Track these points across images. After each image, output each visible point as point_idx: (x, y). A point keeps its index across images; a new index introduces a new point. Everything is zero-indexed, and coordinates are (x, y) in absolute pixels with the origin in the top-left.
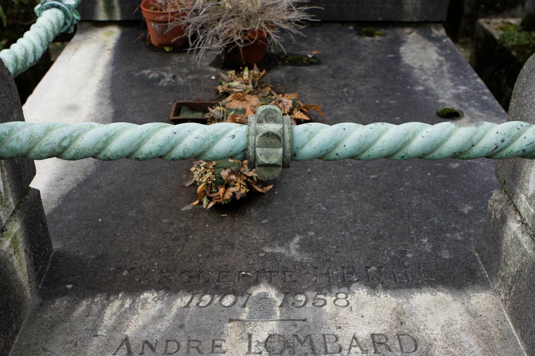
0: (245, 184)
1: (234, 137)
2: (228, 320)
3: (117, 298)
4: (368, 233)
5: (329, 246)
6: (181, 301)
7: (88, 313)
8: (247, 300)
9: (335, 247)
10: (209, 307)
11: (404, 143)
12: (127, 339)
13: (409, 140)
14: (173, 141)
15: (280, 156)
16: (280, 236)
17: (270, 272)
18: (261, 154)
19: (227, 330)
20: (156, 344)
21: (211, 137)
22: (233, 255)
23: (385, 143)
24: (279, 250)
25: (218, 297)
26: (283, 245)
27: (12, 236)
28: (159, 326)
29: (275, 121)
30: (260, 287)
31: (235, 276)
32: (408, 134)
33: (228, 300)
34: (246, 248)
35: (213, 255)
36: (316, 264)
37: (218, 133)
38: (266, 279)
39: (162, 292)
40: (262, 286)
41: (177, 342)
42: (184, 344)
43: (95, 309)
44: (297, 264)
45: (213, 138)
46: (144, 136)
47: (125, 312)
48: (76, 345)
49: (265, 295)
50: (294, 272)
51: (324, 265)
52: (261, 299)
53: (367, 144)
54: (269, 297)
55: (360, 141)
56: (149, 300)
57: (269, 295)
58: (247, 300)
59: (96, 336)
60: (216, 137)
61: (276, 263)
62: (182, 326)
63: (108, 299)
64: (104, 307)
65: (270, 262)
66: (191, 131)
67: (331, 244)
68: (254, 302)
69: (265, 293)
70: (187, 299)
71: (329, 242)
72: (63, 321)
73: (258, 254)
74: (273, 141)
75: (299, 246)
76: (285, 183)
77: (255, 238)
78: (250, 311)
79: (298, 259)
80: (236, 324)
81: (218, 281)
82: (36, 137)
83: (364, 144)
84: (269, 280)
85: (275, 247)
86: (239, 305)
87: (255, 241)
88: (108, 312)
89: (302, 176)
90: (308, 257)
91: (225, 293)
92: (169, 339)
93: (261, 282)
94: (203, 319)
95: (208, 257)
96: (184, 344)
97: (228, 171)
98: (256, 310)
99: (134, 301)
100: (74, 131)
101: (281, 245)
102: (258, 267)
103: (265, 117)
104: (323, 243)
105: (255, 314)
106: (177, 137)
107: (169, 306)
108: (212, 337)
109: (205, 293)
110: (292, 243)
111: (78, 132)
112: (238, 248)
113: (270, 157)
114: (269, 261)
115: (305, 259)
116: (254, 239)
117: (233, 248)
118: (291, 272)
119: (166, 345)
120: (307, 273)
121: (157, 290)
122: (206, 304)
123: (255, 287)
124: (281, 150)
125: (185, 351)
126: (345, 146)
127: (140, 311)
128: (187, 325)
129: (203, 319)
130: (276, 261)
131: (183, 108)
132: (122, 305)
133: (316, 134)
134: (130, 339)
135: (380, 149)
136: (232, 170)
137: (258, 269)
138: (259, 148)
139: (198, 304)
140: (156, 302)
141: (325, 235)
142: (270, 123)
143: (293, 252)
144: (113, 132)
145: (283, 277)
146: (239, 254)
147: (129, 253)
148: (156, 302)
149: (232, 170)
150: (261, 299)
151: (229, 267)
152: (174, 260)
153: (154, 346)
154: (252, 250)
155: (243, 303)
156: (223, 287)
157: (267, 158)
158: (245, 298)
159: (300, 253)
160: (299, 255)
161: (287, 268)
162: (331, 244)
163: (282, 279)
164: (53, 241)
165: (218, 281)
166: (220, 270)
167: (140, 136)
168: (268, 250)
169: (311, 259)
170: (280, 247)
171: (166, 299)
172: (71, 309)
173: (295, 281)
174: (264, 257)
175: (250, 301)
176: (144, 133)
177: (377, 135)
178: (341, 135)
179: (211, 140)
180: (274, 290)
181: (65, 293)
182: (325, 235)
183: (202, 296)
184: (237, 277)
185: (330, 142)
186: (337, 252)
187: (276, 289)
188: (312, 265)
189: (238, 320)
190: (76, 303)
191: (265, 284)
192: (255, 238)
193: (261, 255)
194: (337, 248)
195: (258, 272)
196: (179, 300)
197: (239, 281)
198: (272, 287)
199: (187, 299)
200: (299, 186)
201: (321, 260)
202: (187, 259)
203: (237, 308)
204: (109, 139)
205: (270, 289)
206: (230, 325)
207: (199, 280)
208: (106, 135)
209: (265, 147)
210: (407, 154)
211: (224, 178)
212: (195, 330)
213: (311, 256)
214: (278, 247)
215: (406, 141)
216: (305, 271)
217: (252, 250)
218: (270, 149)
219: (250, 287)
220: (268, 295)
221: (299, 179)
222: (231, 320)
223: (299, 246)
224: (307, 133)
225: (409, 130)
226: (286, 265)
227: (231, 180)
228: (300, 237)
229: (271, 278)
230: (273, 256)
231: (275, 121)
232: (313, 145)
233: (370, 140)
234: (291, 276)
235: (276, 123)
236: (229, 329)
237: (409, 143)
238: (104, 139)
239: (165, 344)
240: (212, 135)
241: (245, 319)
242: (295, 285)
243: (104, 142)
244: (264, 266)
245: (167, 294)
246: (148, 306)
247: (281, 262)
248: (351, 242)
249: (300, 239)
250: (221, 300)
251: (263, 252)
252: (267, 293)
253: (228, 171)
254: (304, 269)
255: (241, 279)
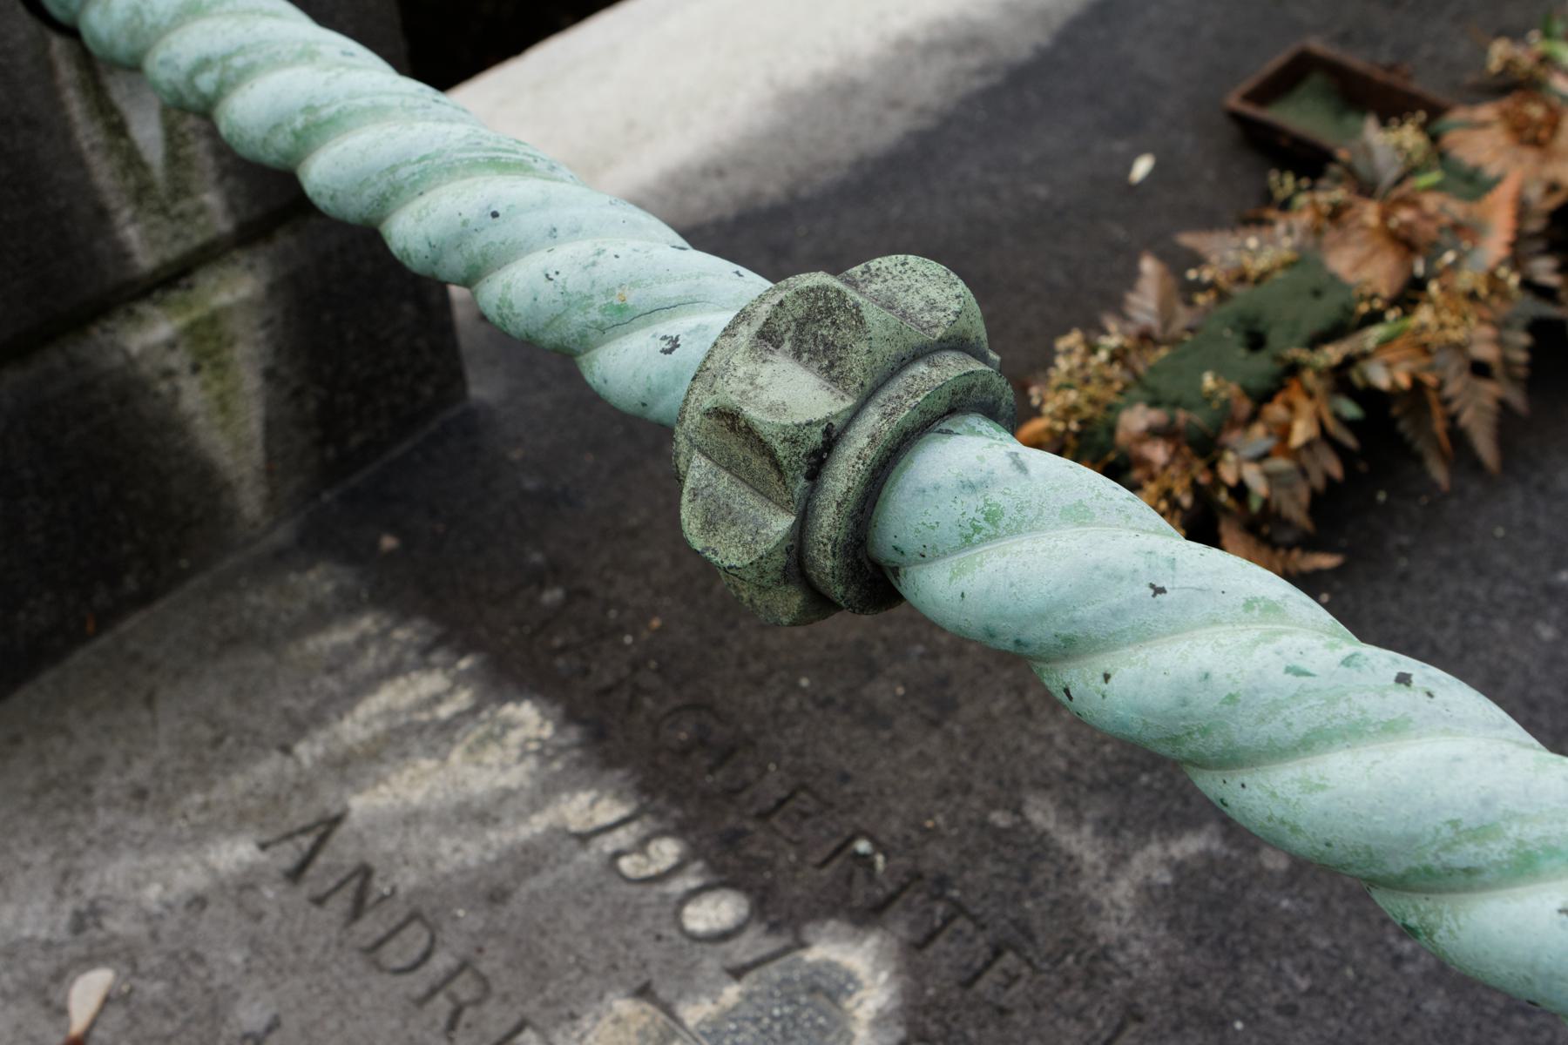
0: (1186, 501)
1: (674, 344)
2: (637, 984)
3: (446, 667)
4: (1519, 1021)
5: (1287, 965)
6: (590, 807)
7: (338, 663)
8: (773, 957)
9: (1303, 984)
10: (635, 890)
11: (1428, 870)
12: (332, 822)
13: (1469, 871)
14: (477, 244)
15: (762, 548)
16: (1148, 788)
17: (959, 909)
18: (695, 493)
19: (598, 1018)
20: (383, 898)
21: (600, 301)
22: (906, 755)
23: (1317, 800)
24: (1083, 845)
25: (700, 873)
26: (1115, 834)
27: (196, 313)
28: (445, 846)
29: (832, 366)
30: (863, 939)
31: (833, 835)
32: (1481, 833)
33: (715, 912)
34: (974, 755)
35: (847, 709)
36: (1151, 1002)
37: (632, 297)
38: (913, 925)
39: (573, 734)
40: (872, 941)
41: (433, 940)
42: (441, 962)
43: (371, 659)
44: (1082, 944)
45: (602, 311)
46: (403, 173)
47: (421, 729)
48: (217, 742)
49: (842, 988)
50: (1036, 970)
51: (1177, 1028)
52: (813, 989)
53: (1217, 742)
54: (849, 1004)
55: (1184, 703)
56: (514, 737)
57: (858, 996)
58: (773, 957)
59: (286, 750)
60: (621, 309)
61: (1016, 886)
62: (497, 896)
63: (426, 651)
64: (395, 670)
65: (1001, 868)
66: (560, 232)
67: (1302, 959)
68: (786, 981)
69: (850, 977)
70: (607, 811)
71: (1306, 946)
72: (268, 643)
73: (992, 805)
74: (757, 463)
75: (1167, 879)
76: (1404, 577)
77: (1049, 738)
78: (735, 1008)
79: (1108, 930)
80: (645, 1019)
81: (763, 816)
82: (149, 19)
83: (1205, 732)
84: (918, 937)
85: (1078, 821)
86: (727, 955)
87: (1035, 749)
88: (387, 697)
89: (1507, 589)
90: (1155, 945)
91: (722, 879)
92: (426, 910)
93: (884, 926)
94: (577, 919)
95: (827, 703)
96: (441, 962)
97: (1156, 416)
98: (756, 1021)
99: (474, 711)
100: (241, 50)
101: (1109, 828)
102: (939, 856)
103: (801, 325)
104: (1275, 934)
105: (737, 1032)
106: (495, 234)
107: (547, 790)
108: (532, 1007)
109: (679, 831)
110: (1155, 850)
111: (252, 57)
112: (949, 737)
113: (722, 527)
114: (1001, 859)
115: (1135, 948)
116: (1037, 737)
117: (935, 724)
118: (1029, 962)
119: (401, 927)
120: (1079, 1015)
121: (571, 716)
122: (643, 873)
123: (846, 928)
124: (781, 524)
125: (420, 989)
126: (1107, 677)
127: (456, 756)
128: (516, 906)
129: (577, 919)
130: (1026, 878)
131: (1317, 79)
132: (437, 699)
133: (1015, 530)
134: (343, 830)
135: (1278, 813)
136: (1172, 421)
137: (927, 865)
138: (703, 461)
139: (618, 854)
140: (521, 759)
141: (1325, 903)
142: (806, 366)
143: (1123, 890)
144: (333, 109)
145: (979, 963)
146: (924, 760)
147: (633, 533)
148: (521, 759)
149: (1172, 421)
150: (813, 989)
151: (848, 789)
152: (719, 643)
153: (371, 899)
154: (987, 777)
155: (748, 959)
156: (753, 850)
157: (709, 525)
158: (770, 945)
159: (1142, 913)
160: (1127, 916)
161: (1031, 938)
162: (1302, 959)
163: (968, 967)
164: (471, 375)
165: (763, 816)
166: (809, 780)
167: (393, 169)
168: (1041, 814)
169: (1157, 966)
170: (1096, 833)
171: (557, 766)
172: (321, 618)
173: (1002, 1011)
174: (998, 834)
175: (774, 971)
176: (409, 162)
177: (1300, 730)
178: (1117, 613)
179: (595, 315)
180: (894, 988)
181: (355, 554)
182: (1325, 903)
183: (662, 834)
184: (835, 843)
185: (1041, 616)
186: (1289, 1010)
187: (904, 993)
188: (1131, 992)
189: (668, 1009)
190: (349, 606)
191: (892, 943)
192: (1049, 738)
193: (1000, 818)
194: (1310, 992)
195: (918, 876)
196: (584, 798)
197: (823, 864)
198: (898, 972)
199: (607, 811)
200: (1442, 624)
201: (1189, 998)
202: (756, 668)
203: (711, 963)
204: (316, 128)
205: (883, 976)
206: (624, 1006)
207: (711, 770)
208: (309, 109)
209: (728, 469)
210: (1430, 935)
211: (1121, 436)
212: (518, 942)
213: (1166, 955)
214: (1087, 830)
215: (1450, 871)
216: (1083, 999)
217: (987, 777)
218: (744, 488)
219: (833, 911)
220: (850, 994)
221: (1480, 592)
222: (643, 992)
223: (1167, 879)
224: (971, 506)
225: (1510, 816)
226: (1037, 923)
227: (1145, 463)
228: (1216, 845)
229: (931, 937)
230: (1041, 847)
231: (832, 366)
232: (963, 583)
233: (1245, 730)
234: (1013, 979)
235: (833, 380)
236: (607, 1020)
237: (1468, 889)
238: (299, 122)
239: (400, 918)
240: (608, 292)
241: (690, 1023)
242: (982, 1026)
243: (297, 135)
244: (963, 868)
245: (576, 753)
246: (492, 755)
247: (1035, 894)
248: (1399, 1008)
249: (1206, 855)
250: (693, 895)
251: (1017, 810)
252: (859, 985)
253: (1156, 416)
254: (1087, 988)
255: (837, 862)
